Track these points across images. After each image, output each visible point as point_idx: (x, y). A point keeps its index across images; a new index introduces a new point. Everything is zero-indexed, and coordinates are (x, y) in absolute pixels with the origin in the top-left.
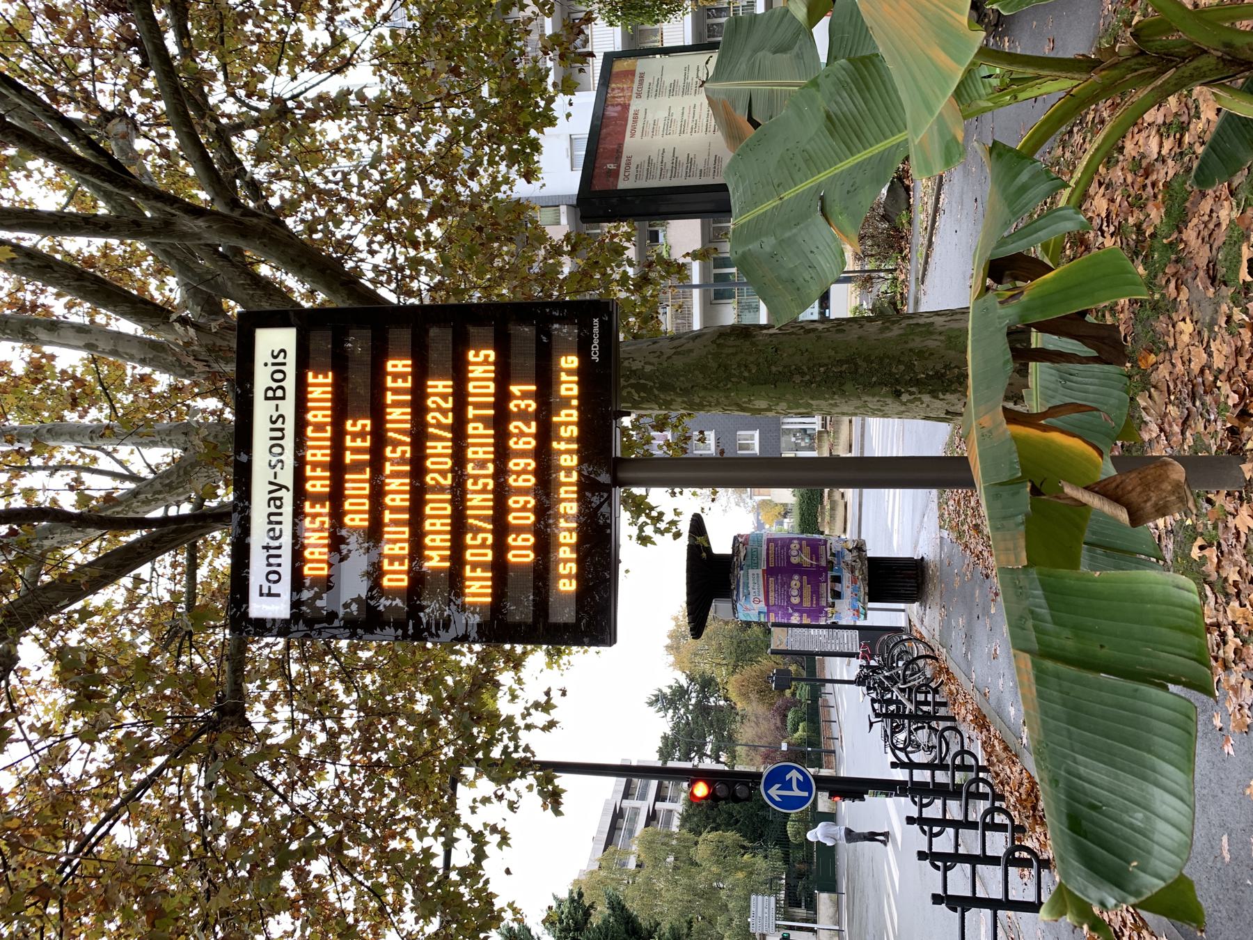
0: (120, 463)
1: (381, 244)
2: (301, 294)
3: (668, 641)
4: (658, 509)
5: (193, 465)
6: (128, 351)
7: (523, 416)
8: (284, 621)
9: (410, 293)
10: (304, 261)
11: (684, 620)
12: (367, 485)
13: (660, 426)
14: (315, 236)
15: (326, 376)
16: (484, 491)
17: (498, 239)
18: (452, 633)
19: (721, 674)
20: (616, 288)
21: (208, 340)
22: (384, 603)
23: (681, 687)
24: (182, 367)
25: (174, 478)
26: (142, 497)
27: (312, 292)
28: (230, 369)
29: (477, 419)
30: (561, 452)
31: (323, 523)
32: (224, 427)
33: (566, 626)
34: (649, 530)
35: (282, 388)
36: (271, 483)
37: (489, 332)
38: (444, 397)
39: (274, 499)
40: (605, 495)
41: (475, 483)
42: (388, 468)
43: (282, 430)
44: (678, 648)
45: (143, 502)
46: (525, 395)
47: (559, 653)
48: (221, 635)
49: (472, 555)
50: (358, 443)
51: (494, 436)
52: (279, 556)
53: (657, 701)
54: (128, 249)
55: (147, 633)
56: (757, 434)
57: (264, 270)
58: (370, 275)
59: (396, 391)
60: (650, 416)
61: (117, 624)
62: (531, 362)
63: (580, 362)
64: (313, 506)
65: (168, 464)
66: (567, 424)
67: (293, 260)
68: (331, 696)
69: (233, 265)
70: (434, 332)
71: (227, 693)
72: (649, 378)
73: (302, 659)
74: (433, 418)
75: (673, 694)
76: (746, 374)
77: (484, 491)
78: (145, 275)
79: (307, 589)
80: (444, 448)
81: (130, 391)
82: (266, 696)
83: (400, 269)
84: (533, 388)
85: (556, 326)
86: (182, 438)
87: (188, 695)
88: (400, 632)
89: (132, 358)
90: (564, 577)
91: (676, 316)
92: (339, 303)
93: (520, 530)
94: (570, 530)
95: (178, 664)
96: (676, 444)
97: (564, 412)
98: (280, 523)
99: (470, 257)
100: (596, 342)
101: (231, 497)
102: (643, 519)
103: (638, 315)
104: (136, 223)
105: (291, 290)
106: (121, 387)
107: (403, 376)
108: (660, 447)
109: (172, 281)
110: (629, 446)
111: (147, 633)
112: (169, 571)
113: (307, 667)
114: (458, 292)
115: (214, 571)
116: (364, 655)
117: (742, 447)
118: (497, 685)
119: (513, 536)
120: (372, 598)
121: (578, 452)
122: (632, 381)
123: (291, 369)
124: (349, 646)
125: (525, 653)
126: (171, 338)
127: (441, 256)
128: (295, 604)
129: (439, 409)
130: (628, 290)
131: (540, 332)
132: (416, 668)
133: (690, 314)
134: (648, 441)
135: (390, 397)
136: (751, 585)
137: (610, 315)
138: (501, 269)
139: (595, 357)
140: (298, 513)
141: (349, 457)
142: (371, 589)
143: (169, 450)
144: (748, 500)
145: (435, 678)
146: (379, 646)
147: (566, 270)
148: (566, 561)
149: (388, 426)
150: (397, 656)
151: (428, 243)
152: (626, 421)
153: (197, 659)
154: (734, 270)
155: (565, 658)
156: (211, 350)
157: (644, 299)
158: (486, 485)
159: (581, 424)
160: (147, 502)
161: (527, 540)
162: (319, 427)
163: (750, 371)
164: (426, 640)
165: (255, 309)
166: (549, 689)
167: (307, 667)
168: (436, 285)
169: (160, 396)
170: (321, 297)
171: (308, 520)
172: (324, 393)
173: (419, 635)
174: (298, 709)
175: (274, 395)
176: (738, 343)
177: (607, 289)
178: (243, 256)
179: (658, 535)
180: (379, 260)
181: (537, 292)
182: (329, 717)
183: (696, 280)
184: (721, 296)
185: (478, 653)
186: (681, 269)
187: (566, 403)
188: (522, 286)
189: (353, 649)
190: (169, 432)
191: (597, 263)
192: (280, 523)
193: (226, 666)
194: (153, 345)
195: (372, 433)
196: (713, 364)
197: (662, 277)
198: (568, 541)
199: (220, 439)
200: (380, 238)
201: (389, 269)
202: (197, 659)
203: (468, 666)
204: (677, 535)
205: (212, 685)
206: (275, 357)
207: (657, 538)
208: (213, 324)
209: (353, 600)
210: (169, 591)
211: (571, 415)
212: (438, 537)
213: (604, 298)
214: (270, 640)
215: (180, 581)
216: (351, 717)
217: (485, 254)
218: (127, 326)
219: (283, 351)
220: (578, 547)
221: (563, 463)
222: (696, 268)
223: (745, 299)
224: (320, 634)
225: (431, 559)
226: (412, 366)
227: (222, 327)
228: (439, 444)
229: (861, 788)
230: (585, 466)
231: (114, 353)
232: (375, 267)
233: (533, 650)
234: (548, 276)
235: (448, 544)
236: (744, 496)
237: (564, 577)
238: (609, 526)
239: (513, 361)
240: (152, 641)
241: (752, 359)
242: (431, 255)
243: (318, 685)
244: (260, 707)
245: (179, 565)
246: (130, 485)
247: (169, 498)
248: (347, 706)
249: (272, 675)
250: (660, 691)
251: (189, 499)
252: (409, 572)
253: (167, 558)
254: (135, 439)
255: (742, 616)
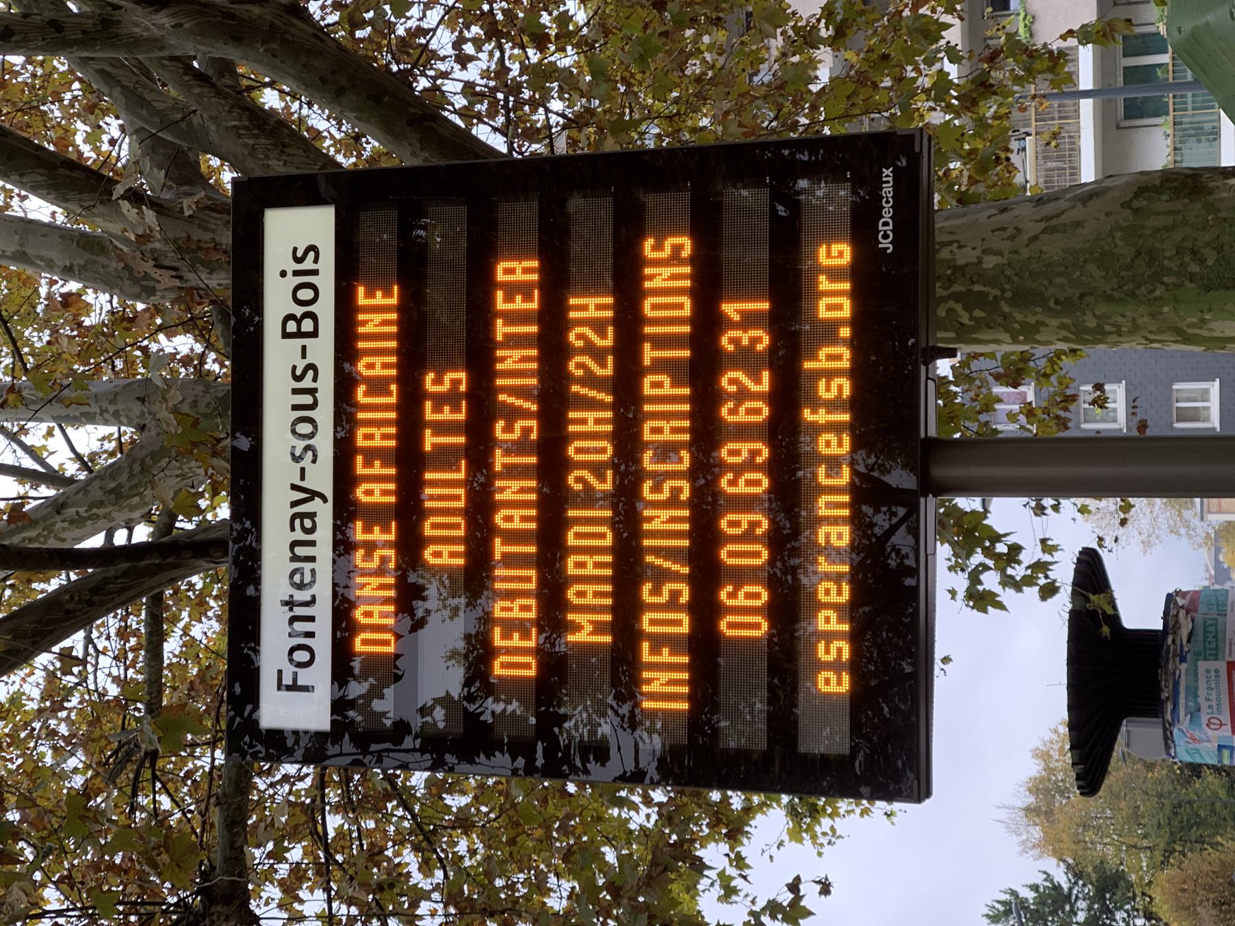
0: (31, 451)
1: (478, 43)
2: (336, 143)
3: (1030, 800)
4: (1011, 540)
5: (156, 456)
6: (43, 253)
7: (746, 359)
8: (319, 736)
9: (532, 134)
10: (344, 82)
11: (1063, 759)
12: (461, 492)
13: (1013, 375)
14: (359, 34)
15: (388, 293)
16: (673, 502)
17: (693, 21)
18: (615, 767)
19: (1138, 868)
20: (922, 104)
21: (177, 231)
22: (493, 707)
23: (1057, 888)
24: (135, 280)
25: (123, 478)
26: (70, 512)
27: (357, 138)
28: (220, 282)
29: (660, 366)
30: (817, 429)
31: (384, 560)
32: (207, 386)
33: (825, 760)
34: (990, 580)
35: (312, 316)
36: (294, 487)
37: (679, 202)
38: (598, 326)
39: (302, 516)
40: (901, 512)
41: (657, 488)
42: (500, 460)
43: (312, 392)
44: (1049, 814)
45: (72, 522)
46: (749, 320)
47: (815, 813)
48: (215, 757)
49: (653, 622)
50: (447, 415)
51: (692, 399)
52: (311, 619)
53: (1007, 913)
54: (40, 71)
55: (80, 753)
56: (1214, 388)
57: (270, 99)
58: (460, 102)
59: (513, 318)
60: (992, 356)
61: (30, 736)
62: (760, 256)
63: (855, 255)
64: (368, 529)
65: (112, 454)
66: (830, 374)
67: (323, 80)
68: (397, 876)
69: (219, 93)
70: (576, 204)
71: (218, 862)
72: (992, 279)
73: (346, 806)
74: (579, 366)
75: (1041, 900)
76: (1195, 268)
77: (673, 502)
78: (70, 118)
79: (355, 678)
80: (598, 421)
81: (45, 324)
82: (283, 870)
83: (515, 89)
84: (766, 306)
85: (803, 183)
86: (137, 408)
87: (154, 866)
88: (520, 762)
89: (50, 266)
90: (828, 666)
91: (1044, 155)
92: (405, 157)
93: (740, 576)
94: (837, 578)
95: (133, 811)
96: (1046, 411)
97: (823, 352)
98: (312, 559)
99: (642, 60)
100: (887, 214)
101: (224, 512)
102: (978, 558)
103: (968, 157)
104: (56, 25)
105: (318, 134)
106: (30, 317)
107: (524, 289)
108: (1012, 417)
109: (113, 126)
110: (949, 416)
111: (80, 753)
112: (115, 644)
113: (356, 821)
114: (621, 127)
115: (190, 644)
116: (455, 801)
117: (1184, 415)
118: (699, 867)
119: (730, 588)
120: (470, 698)
121: (852, 428)
122: (957, 288)
123: (326, 282)
124: (429, 784)
125: (748, 810)
126: (115, 228)
127: (590, 63)
128: (339, 706)
129: (590, 350)
130: (948, 108)
131: (776, 197)
132: (549, 829)
133: (1075, 150)
134: (988, 405)
135: (501, 329)
136: (1202, 692)
137: (915, 159)
138: (699, 79)
139: (886, 244)
140: (343, 546)
141: (430, 441)
142: (468, 683)
143: (105, 430)
144: (1196, 522)
145: (584, 848)
146: (482, 786)
147: (824, 75)
148: (830, 636)
149: (500, 382)
150: (514, 805)
151: (565, 36)
152: (944, 367)
153: (165, 803)
154: (1165, 58)
155: (826, 823)
156: (185, 248)
157: (981, 123)
158: (676, 491)
159: (857, 373)
160: (78, 522)
161: (757, 596)
162: (378, 386)
163: (1202, 262)
164: (565, 777)
165: (259, 173)
166: (798, 879)
167: (356, 821)
168: (579, 116)
169: (94, 330)
170: (371, 145)
171: (360, 554)
172: (385, 323)
173: (557, 768)
174: (339, 895)
175: (298, 328)
176: (1177, 205)
177: (905, 107)
178: (236, 76)
179: (1010, 592)
180: (473, 73)
181: (767, 119)
182: (394, 914)
183: (1086, 81)
184: (1137, 110)
185: (660, 805)
186: (1057, 62)
187: (828, 332)
188: (739, 110)
189: (436, 789)
190: (114, 397)
191: (885, 57)
192: (312, 559)
193: (216, 816)
194: (87, 243)
195: (470, 396)
196: (1125, 251)
197: (1018, 80)
198: (834, 598)
199: (202, 408)
200: (476, 30)
201: (493, 90)
202: (165, 803)
203: (642, 828)
204: (1049, 591)
205: (193, 849)
206: (299, 260)
207: (1007, 596)
208: (186, 202)
209: (437, 701)
210: (116, 680)
211: (838, 357)
212: (590, 589)
213: (902, 127)
214: (290, 769)
215: (134, 662)
216: (433, 914)
217: (669, 53)
218: (39, 209)
219: (312, 248)
220: (851, 611)
221: (823, 450)
222: (1086, 57)
223: (1189, 116)
224: (379, 761)
225: (578, 628)
226: (541, 270)
227: (203, 208)
228: (590, 416)
229: (463, 112)
230: (862, 453)
231: (21, 257)
232: (469, 87)
233: (762, 805)
234: (790, 89)
235: (608, 601)
236: (1187, 514)
237: (828, 666)
238: (914, 572)
239: (728, 254)
240: (88, 767)
241: (1206, 237)
242: (567, 59)
243: (375, 854)
244: (273, 892)
245: (136, 633)
246: (46, 491)
247: (115, 515)
248: (426, 895)
249: (294, 834)
250: (1014, 893)
251: (147, 518)
252: (538, 652)
253: (112, 623)
254: (57, 409)
255: (1183, 754)
